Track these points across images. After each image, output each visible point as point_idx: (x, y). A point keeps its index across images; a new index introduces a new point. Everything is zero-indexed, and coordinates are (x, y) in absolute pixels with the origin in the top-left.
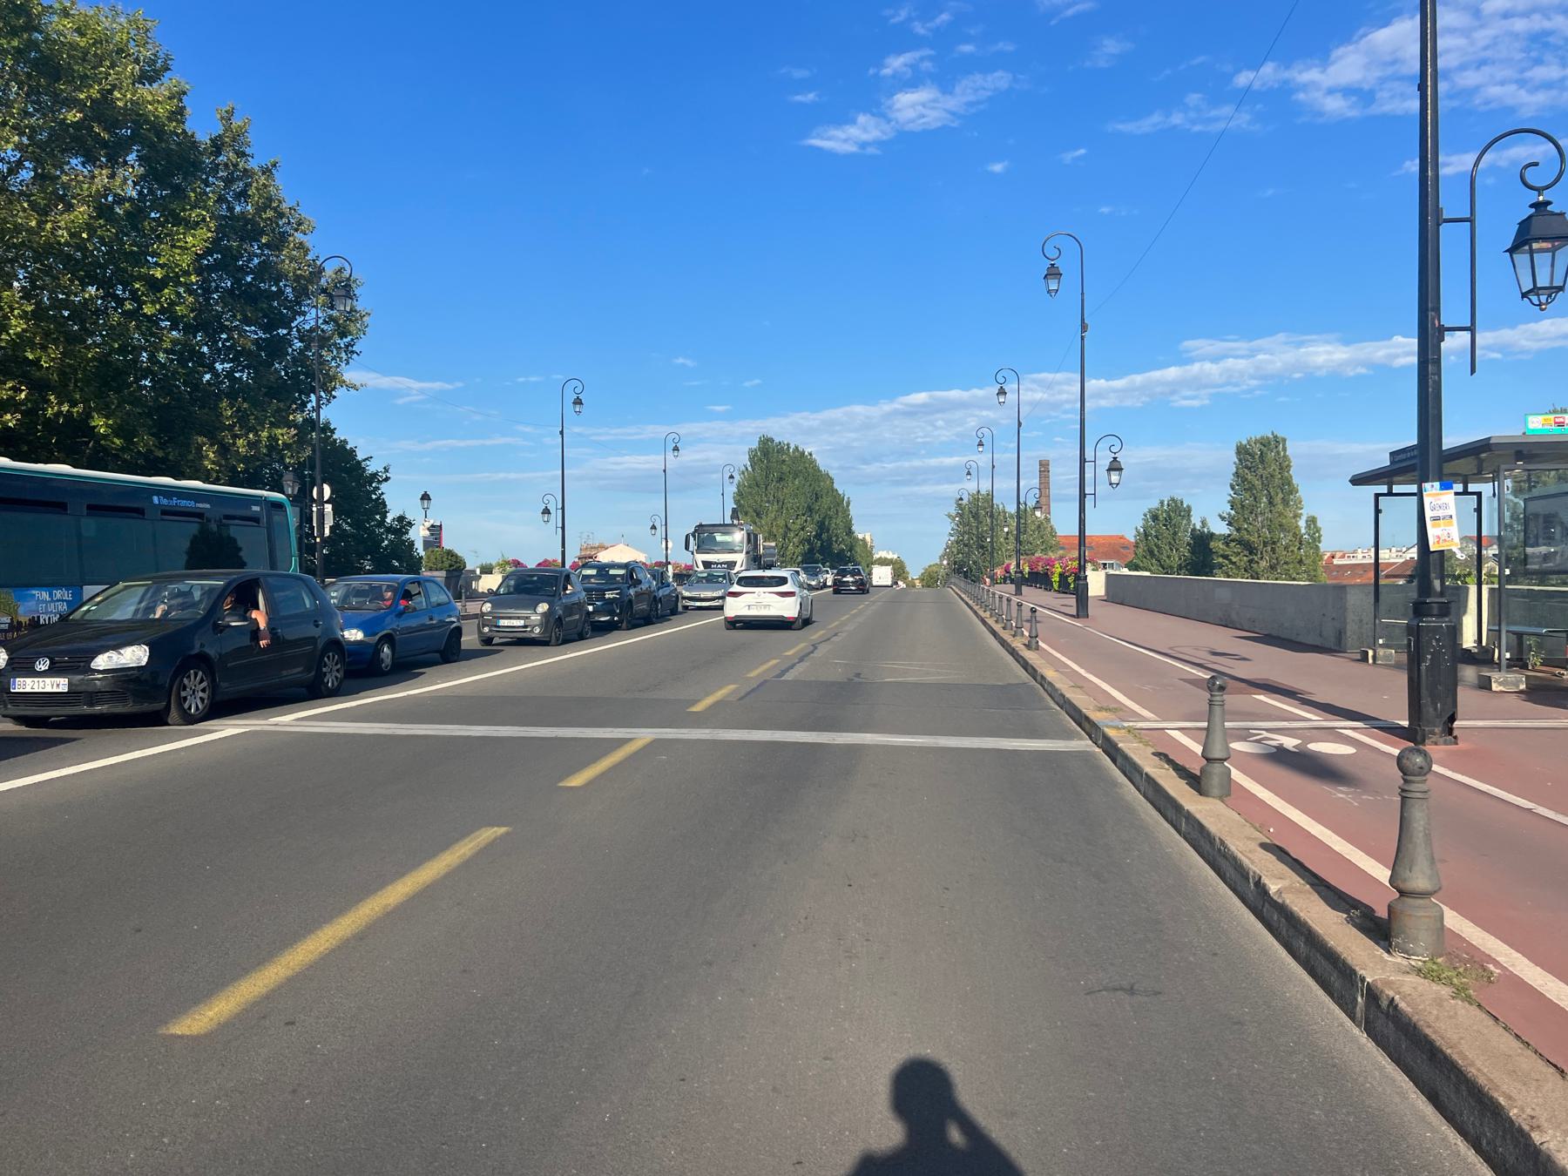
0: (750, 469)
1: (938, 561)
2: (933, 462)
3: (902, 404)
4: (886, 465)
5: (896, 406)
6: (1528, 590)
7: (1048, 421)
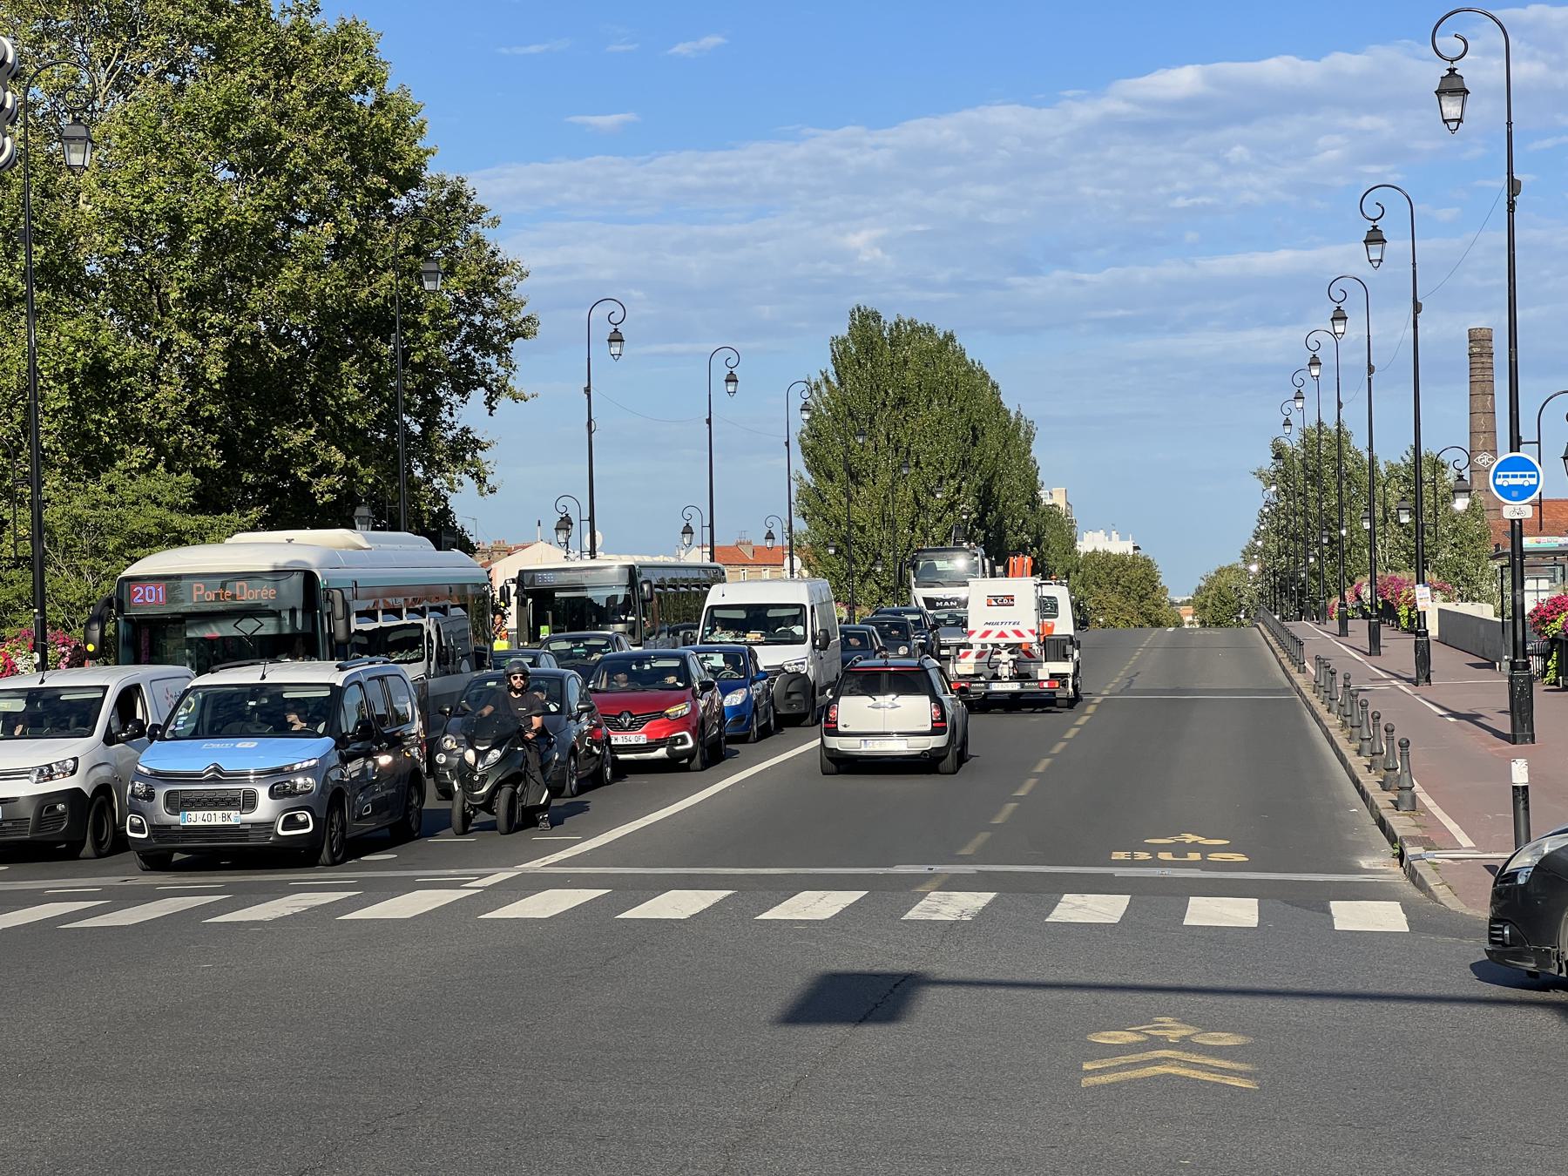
0: (833, 378)
1: (1236, 559)
2: (1225, 265)
3: (1127, 100)
4: (1085, 276)
5: (1112, 105)
6: (584, 630)
7: (1549, 143)
